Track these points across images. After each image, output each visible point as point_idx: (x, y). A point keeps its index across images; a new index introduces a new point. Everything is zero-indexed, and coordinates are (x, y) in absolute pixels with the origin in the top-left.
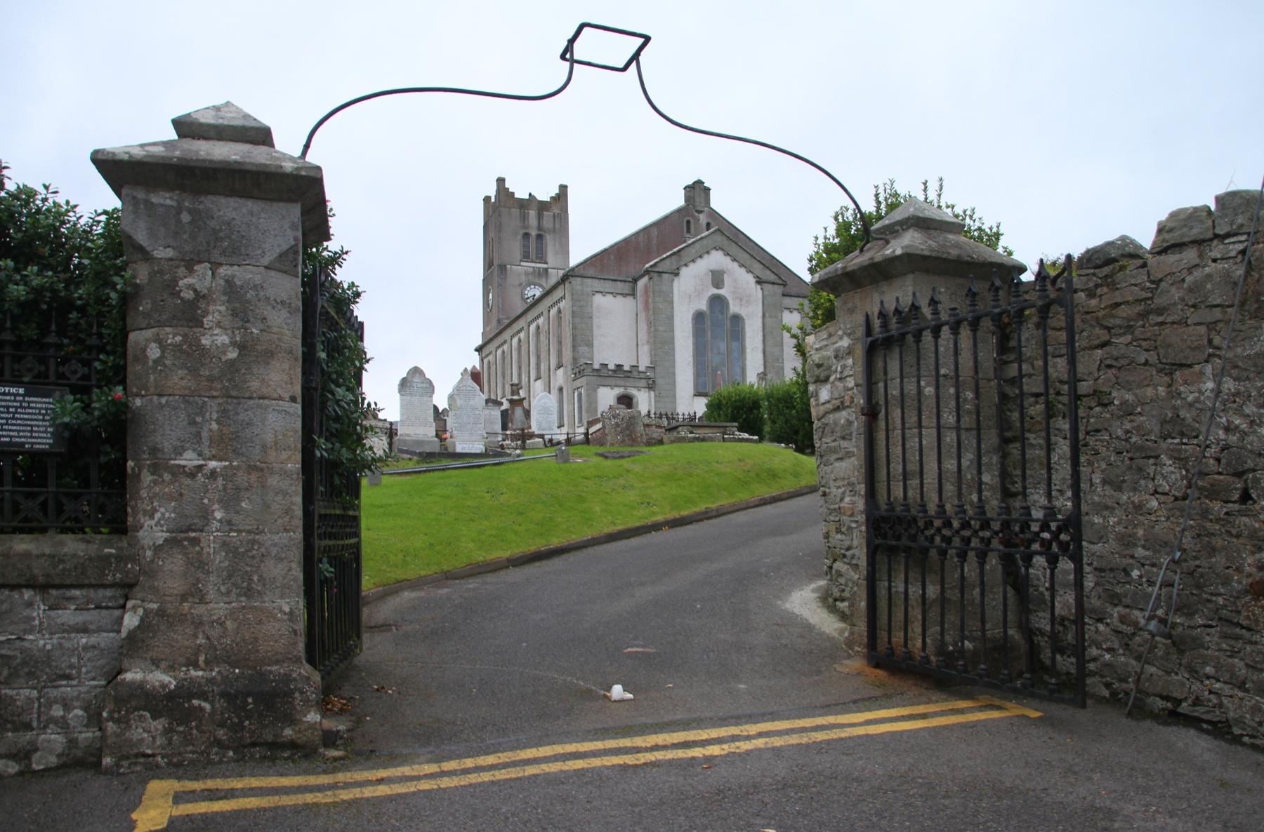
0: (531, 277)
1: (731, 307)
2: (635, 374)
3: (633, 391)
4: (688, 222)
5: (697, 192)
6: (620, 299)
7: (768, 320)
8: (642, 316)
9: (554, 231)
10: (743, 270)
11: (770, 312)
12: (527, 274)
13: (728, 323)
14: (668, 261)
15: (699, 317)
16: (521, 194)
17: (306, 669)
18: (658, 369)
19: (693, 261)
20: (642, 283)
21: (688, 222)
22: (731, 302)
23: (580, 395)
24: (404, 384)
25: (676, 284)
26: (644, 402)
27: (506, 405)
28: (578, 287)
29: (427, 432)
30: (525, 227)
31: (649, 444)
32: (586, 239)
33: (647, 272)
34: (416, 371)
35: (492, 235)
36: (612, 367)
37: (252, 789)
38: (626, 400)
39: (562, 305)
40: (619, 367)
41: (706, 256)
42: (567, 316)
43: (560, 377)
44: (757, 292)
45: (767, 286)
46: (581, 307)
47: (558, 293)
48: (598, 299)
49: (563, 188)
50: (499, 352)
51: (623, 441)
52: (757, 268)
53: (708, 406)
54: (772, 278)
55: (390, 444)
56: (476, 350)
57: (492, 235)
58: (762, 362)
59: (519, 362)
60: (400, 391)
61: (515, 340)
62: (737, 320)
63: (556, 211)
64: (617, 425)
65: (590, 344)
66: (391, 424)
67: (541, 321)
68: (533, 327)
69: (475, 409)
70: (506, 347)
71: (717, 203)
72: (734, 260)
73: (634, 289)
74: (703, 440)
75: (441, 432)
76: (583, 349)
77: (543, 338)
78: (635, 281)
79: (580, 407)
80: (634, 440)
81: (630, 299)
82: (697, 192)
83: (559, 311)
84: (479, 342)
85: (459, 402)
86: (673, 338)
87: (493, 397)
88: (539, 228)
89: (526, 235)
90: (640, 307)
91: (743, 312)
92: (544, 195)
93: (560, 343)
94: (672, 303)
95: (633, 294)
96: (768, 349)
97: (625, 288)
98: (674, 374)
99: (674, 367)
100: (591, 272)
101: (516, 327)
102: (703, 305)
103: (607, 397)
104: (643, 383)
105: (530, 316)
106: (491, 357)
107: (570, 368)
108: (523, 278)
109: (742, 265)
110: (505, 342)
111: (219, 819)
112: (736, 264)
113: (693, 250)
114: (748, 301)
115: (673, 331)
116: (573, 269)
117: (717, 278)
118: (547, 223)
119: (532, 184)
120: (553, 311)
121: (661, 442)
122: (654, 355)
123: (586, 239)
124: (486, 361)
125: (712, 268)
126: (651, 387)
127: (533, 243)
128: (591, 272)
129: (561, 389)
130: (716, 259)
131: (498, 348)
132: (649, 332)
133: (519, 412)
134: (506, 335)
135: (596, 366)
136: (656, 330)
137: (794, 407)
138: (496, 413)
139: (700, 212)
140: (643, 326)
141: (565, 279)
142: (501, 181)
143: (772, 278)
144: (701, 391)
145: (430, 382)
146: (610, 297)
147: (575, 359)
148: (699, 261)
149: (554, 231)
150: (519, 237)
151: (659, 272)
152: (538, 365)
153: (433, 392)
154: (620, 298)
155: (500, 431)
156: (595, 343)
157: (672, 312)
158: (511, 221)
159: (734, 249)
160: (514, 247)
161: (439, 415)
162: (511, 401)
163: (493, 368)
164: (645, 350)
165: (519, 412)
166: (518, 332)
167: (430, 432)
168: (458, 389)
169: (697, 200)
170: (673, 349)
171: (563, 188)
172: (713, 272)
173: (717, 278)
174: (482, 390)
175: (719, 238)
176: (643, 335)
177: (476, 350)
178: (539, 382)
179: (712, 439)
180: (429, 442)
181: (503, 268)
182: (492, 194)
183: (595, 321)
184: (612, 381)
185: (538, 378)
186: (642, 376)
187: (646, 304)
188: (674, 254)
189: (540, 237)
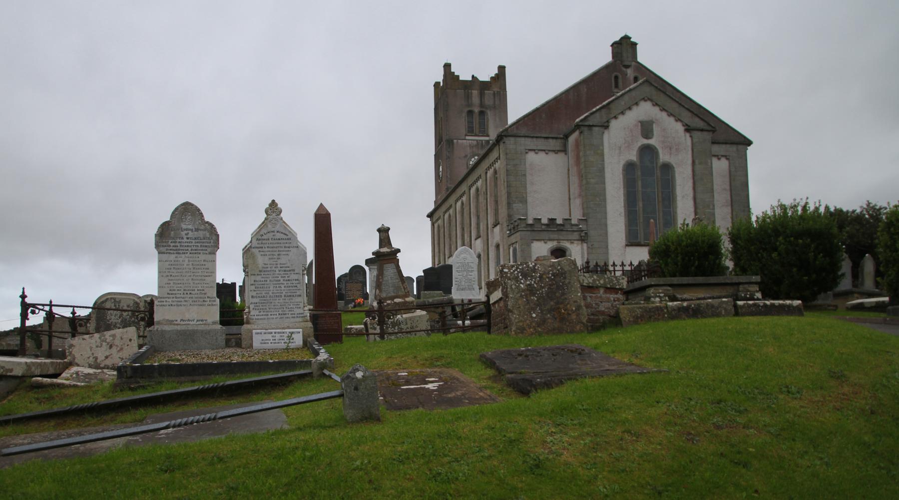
0: (474, 149)
1: (661, 156)
2: (568, 227)
3: (567, 245)
4: (616, 78)
5: (624, 48)
6: (552, 156)
7: (698, 167)
8: (574, 170)
9: (494, 107)
10: (672, 119)
11: (700, 160)
12: (471, 146)
13: (658, 172)
14: (597, 114)
15: (629, 167)
16: (465, 76)
19: (630, 108)
20: (572, 139)
21: (616, 78)
22: (660, 151)
23: (515, 250)
24: (165, 234)
25: (606, 136)
26: (577, 253)
30: (470, 105)
31: (596, 326)
32: (520, 103)
33: (578, 126)
35: (441, 115)
36: (545, 221)
38: (559, 252)
39: (497, 165)
40: (552, 220)
41: (635, 108)
42: (502, 176)
43: (497, 235)
44: (686, 140)
45: (697, 134)
46: (515, 165)
48: (531, 156)
49: (502, 69)
50: (447, 216)
51: (542, 322)
52: (687, 116)
53: (650, 253)
54: (700, 124)
56: (428, 216)
57: (441, 115)
58: (692, 210)
59: (462, 224)
60: (157, 246)
61: (459, 204)
62: (667, 168)
63: (496, 90)
64: (531, 290)
65: (524, 201)
67: (479, 183)
68: (473, 190)
70: (451, 211)
71: (644, 57)
72: (663, 110)
74: (695, 313)
76: (517, 206)
77: (481, 199)
78: (566, 137)
80: (562, 319)
81: (561, 155)
82: (624, 48)
83: (495, 172)
84: (432, 207)
85: (261, 260)
86: (604, 189)
88: (482, 105)
89: (470, 113)
90: (572, 161)
91: (672, 160)
92: (485, 76)
93: (496, 202)
94: (602, 155)
98: (606, 225)
100: (523, 131)
102: (633, 156)
103: (541, 249)
104: (576, 235)
105: (470, 180)
106: (440, 222)
107: (505, 225)
108: (468, 150)
109: (670, 115)
110: (451, 206)
112: (664, 114)
114: (677, 150)
115: (604, 183)
117: (646, 129)
118: (488, 100)
119: (475, 67)
120: (490, 172)
121: (615, 321)
122: (585, 207)
123: (520, 103)
124: (436, 225)
125: (641, 118)
126: (583, 239)
127: (476, 119)
128: (523, 131)
129: (498, 246)
130: (645, 110)
132: (581, 186)
135: (530, 222)
136: (588, 183)
137: (775, 249)
139: (627, 67)
140: (575, 180)
141: (500, 138)
142: (447, 66)
143: (700, 124)
146: (542, 155)
147: (510, 216)
148: (628, 113)
149: (495, 107)
150: (464, 114)
151: (590, 126)
152: (478, 224)
153: (217, 246)
156: (529, 200)
157: (603, 165)
159: (662, 99)
160: (460, 123)
161: (226, 291)
163: (442, 231)
164: (577, 203)
166: (461, 196)
169: (624, 55)
170: (605, 200)
171: (502, 69)
172: (641, 122)
173: (646, 129)
175: (647, 89)
176: (575, 189)
177: (428, 216)
178: (479, 241)
179: (714, 312)
181: (450, 142)
182: (440, 79)
183: (529, 178)
184: (545, 235)
185: (478, 237)
186: (575, 228)
187: (578, 158)
189: (482, 113)
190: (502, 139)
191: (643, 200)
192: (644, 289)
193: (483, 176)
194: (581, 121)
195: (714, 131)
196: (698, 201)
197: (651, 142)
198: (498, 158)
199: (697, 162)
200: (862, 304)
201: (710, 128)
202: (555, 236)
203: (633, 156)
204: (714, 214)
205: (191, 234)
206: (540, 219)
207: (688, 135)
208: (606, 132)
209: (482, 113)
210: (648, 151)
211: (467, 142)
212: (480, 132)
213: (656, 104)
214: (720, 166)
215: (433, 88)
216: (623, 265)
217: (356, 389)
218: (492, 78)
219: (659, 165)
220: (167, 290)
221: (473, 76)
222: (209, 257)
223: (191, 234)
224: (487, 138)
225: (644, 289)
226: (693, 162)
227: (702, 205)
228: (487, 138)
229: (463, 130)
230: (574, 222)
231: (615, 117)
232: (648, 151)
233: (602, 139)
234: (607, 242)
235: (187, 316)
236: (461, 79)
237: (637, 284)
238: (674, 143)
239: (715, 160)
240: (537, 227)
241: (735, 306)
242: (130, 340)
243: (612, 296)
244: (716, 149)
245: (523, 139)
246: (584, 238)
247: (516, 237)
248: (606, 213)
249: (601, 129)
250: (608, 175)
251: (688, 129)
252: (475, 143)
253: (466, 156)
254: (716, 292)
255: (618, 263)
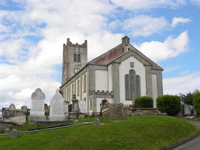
2: (108, 94)
3: (107, 99)
7: (147, 77)
11: (148, 74)
12: (75, 66)
13: (135, 78)
14: (117, 60)
15: (126, 76)
16: (74, 43)
17: (45, 116)
18: (115, 92)
19: (127, 58)
21: (123, 48)
23: (91, 100)
24: (34, 95)
25: (120, 66)
27: (71, 103)
28: (91, 68)
29: (41, 113)
32: (93, 53)
34: (39, 90)
37: (78, 58)
46: (92, 74)
47: (85, 70)
48: (97, 71)
49: (86, 41)
52: (144, 61)
54: (148, 64)
55: (27, 120)
57: (65, 54)
62: (138, 77)
65: (94, 85)
66: (28, 110)
69: (60, 104)
73: (107, 68)
75: (47, 114)
76: (92, 86)
79: (91, 104)
86: (119, 82)
87: (66, 100)
95: (107, 70)
96: (147, 86)
97: (105, 68)
99: (119, 91)
101: (72, 80)
102: (128, 73)
103: (99, 101)
104: (110, 96)
105: (76, 77)
110: (69, 85)
111: (54, 102)
113: (125, 56)
116: (90, 62)
117: (132, 65)
122: (113, 88)
130: (132, 59)
131: (66, 87)
133: (76, 105)
134: (69, 83)
135: (96, 91)
138: (67, 106)
141: (87, 65)
142: (68, 39)
143: (148, 64)
144: (127, 98)
145: (44, 94)
150: (73, 55)
154: (103, 71)
155: (68, 112)
158: (71, 50)
159: (137, 56)
160: (72, 58)
162: (73, 101)
165: (76, 105)
166: (73, 82)
167: (43, 113)
168: (55, 97)
170: (119, 86)
171: (86, 41)
172: (131, 63)
173: (132, 65)
174: (63, 97)
180: (42, 117)
181: (68, 64)
182: (66, 43)
184: (101, 96)
185: (85, 92)
186: (110, 94)
188: (119, 57)
190: (88, 65)
191: (131, 86)
192: (136, 110)
193: (81, 76)
194: (113, 61)
195: (152, 66)
196: (147, 87)
197: (133, 69)
198: (86, 71)
199: (147, 75)
200: (189, 118)
201: (151, 65)
202: (104, 97)
203: (128, 73)
204: (152, 91)
205: (39, 95)
206: (104, 91)
207: (144, 67)
208: (120, 65)
209: (79, 55)
210: (132, 71)
211: (73, 65)
212: (78, 61)
213: (135, 57)
214: (154, 77)
215: (63, 46)
216: (125, 105)
217: (97, 121)
218: (83, 44)
219: (136, 75)
220: (33, 107)
221: (77, 43)
222: (43, 100)
223: (39, 95)
224: (81, 63)
225: (136, 110)
226: (146, 75)
227: (149, 90)
228: (81, 63)
229: (73, 60)
230: (110, 92)
231: (123, 61)
232: (132, 71)
233: (119, 67)
234: (120, 99)
235: (38, 113)
236: (73, 43)
237: (134, 109)
238: (140, 70)
239: (152, 75)
240: (98, 93)
241: (154, 114)
242: (20, 120)
243: (130, 111)
244: (153, 71)
245: (94, 66)
246: (113, 97)
247: (92, 96)
248: (119, 90)
249: (119, 64)
250: (120, 78)
251: (144, 65)
252: (77, 64)
253: (73, 69)
254: (150, 111)
255: (126, 105)
